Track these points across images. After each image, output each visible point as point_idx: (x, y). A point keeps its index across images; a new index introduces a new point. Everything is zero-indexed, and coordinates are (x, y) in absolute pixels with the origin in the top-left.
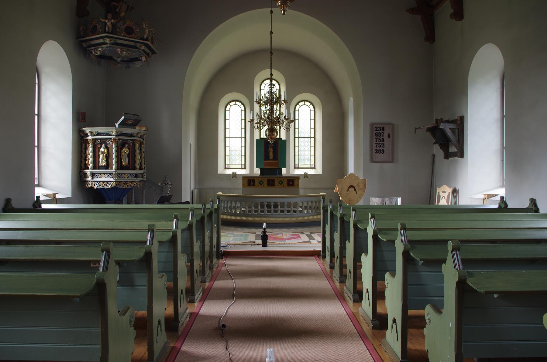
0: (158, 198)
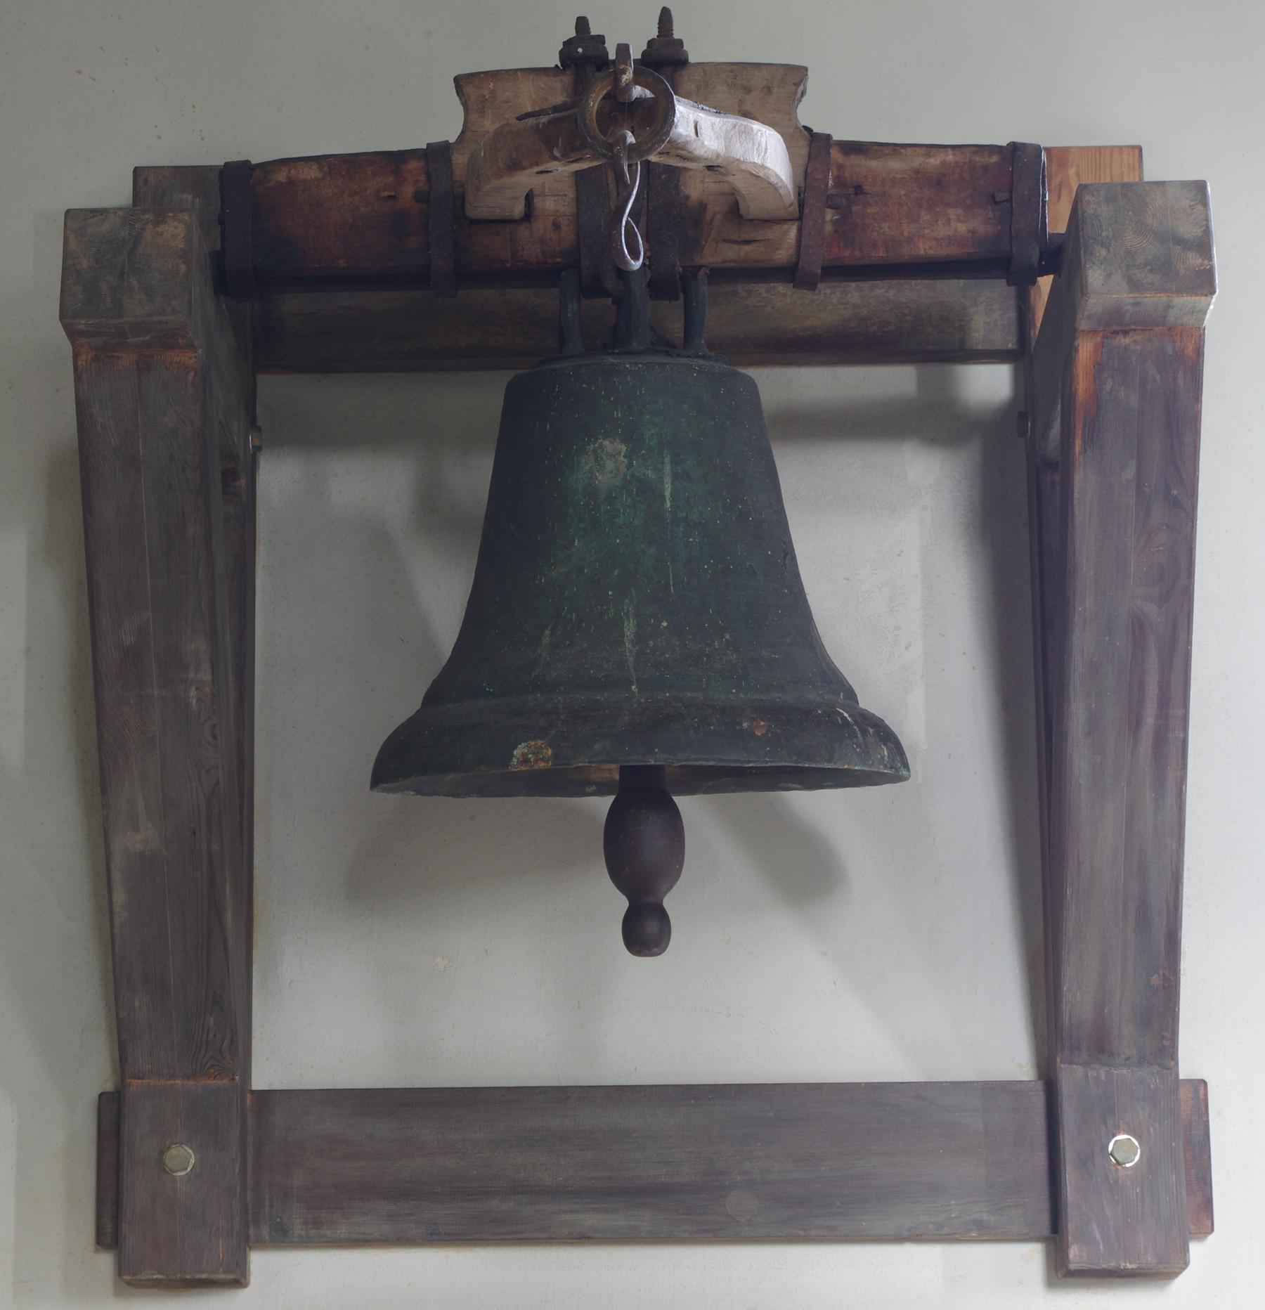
0: (1200, 207)
